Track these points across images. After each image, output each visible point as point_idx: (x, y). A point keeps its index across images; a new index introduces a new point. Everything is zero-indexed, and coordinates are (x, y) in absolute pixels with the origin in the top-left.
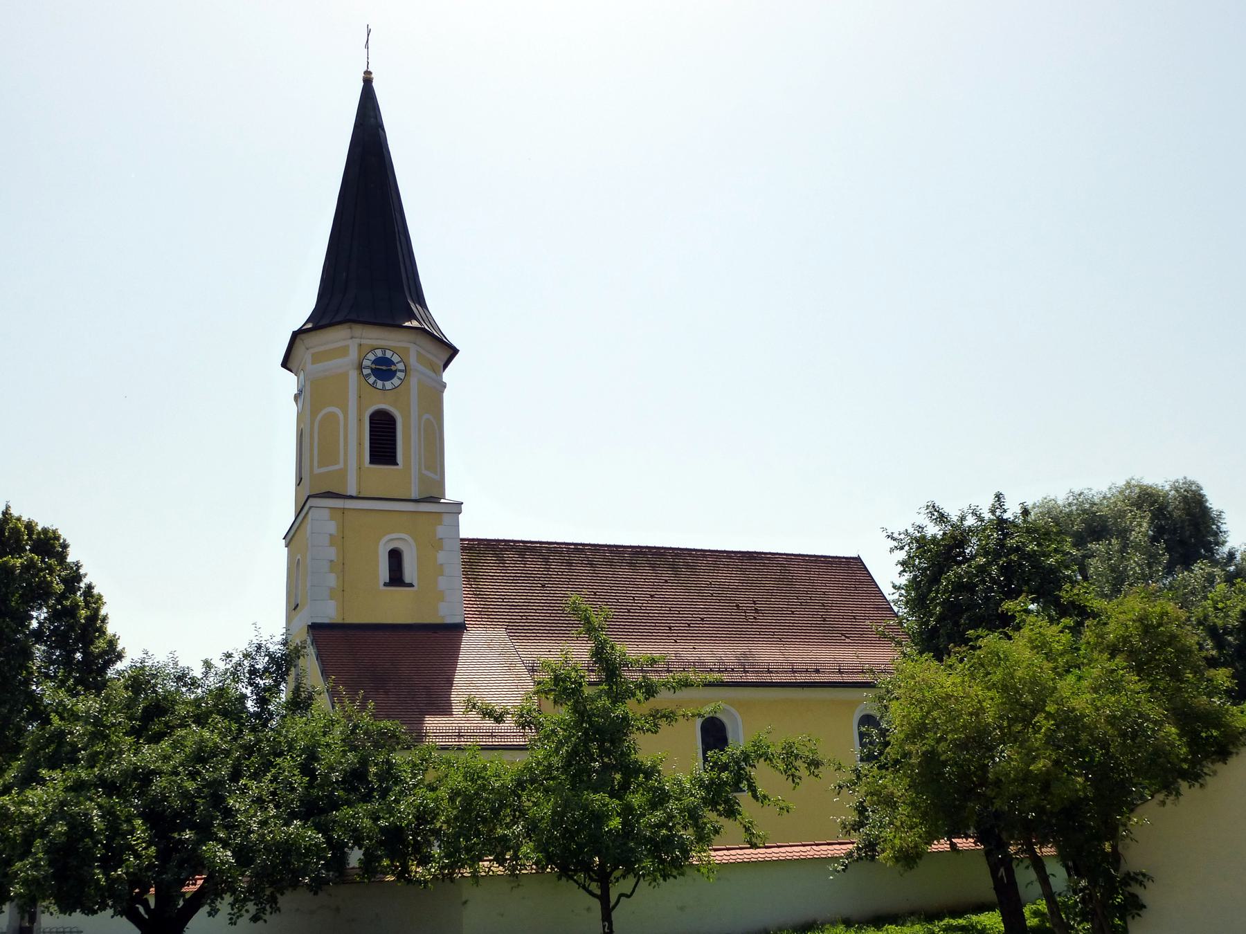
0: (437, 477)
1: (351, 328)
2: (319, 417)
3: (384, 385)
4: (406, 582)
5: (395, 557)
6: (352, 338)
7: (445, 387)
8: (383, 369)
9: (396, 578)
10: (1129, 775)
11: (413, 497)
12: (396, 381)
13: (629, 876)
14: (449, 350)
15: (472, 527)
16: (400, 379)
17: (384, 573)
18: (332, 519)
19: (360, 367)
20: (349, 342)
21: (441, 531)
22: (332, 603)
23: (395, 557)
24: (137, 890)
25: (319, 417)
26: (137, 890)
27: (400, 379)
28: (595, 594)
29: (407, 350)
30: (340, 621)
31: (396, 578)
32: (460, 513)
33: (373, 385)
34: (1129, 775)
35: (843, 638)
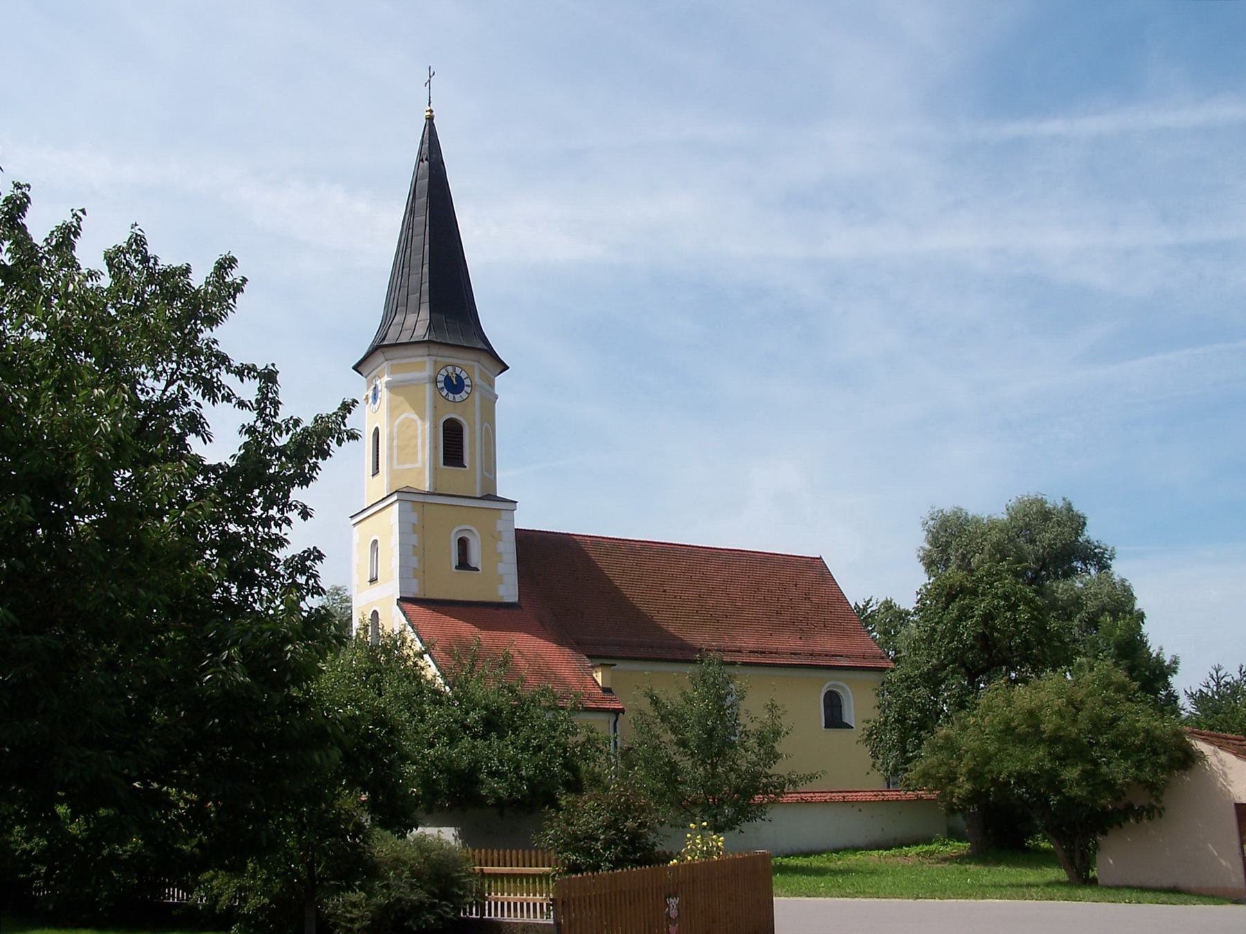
0: (492, 477)
1: (428, 347)
2: (397, 422)
3: (454, 397)
4: (473, 566)
5: (463, 544)
6: (429, 355)
7: (497, 398)
8: (454, 385)
9: (464, 564)
10: (136, 492)
11: (478, 496)
12: (464, 395)
13: (1169, 680)
14: (501, 366)
15: (525, 520)
16: (466, 392)
17: (455, 560)
18: (414, 511)
19: (436, 381)
20: (426, 359)
21: (500, 525)
22: (415, 581)
23: (463, 544)
24: (164, 822)
25: (397, 422)
26: (164, 822)
27: (466, 392)
28: (697, 612)
29: (473, 367)
30: (421, 596)
31: (464, 564)
32: (514, 510)
33: (446, 398)
34: (136, 492)
35: (813, 627)
